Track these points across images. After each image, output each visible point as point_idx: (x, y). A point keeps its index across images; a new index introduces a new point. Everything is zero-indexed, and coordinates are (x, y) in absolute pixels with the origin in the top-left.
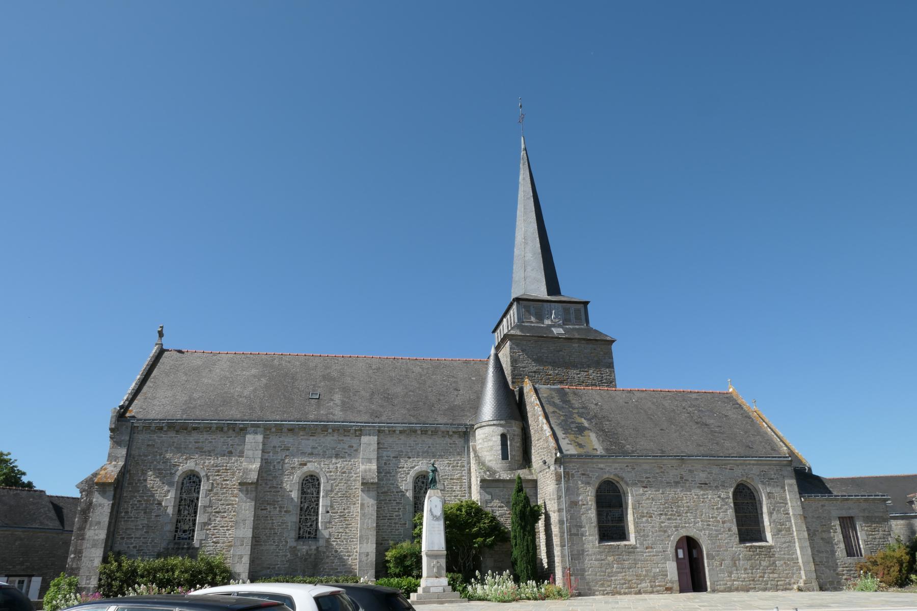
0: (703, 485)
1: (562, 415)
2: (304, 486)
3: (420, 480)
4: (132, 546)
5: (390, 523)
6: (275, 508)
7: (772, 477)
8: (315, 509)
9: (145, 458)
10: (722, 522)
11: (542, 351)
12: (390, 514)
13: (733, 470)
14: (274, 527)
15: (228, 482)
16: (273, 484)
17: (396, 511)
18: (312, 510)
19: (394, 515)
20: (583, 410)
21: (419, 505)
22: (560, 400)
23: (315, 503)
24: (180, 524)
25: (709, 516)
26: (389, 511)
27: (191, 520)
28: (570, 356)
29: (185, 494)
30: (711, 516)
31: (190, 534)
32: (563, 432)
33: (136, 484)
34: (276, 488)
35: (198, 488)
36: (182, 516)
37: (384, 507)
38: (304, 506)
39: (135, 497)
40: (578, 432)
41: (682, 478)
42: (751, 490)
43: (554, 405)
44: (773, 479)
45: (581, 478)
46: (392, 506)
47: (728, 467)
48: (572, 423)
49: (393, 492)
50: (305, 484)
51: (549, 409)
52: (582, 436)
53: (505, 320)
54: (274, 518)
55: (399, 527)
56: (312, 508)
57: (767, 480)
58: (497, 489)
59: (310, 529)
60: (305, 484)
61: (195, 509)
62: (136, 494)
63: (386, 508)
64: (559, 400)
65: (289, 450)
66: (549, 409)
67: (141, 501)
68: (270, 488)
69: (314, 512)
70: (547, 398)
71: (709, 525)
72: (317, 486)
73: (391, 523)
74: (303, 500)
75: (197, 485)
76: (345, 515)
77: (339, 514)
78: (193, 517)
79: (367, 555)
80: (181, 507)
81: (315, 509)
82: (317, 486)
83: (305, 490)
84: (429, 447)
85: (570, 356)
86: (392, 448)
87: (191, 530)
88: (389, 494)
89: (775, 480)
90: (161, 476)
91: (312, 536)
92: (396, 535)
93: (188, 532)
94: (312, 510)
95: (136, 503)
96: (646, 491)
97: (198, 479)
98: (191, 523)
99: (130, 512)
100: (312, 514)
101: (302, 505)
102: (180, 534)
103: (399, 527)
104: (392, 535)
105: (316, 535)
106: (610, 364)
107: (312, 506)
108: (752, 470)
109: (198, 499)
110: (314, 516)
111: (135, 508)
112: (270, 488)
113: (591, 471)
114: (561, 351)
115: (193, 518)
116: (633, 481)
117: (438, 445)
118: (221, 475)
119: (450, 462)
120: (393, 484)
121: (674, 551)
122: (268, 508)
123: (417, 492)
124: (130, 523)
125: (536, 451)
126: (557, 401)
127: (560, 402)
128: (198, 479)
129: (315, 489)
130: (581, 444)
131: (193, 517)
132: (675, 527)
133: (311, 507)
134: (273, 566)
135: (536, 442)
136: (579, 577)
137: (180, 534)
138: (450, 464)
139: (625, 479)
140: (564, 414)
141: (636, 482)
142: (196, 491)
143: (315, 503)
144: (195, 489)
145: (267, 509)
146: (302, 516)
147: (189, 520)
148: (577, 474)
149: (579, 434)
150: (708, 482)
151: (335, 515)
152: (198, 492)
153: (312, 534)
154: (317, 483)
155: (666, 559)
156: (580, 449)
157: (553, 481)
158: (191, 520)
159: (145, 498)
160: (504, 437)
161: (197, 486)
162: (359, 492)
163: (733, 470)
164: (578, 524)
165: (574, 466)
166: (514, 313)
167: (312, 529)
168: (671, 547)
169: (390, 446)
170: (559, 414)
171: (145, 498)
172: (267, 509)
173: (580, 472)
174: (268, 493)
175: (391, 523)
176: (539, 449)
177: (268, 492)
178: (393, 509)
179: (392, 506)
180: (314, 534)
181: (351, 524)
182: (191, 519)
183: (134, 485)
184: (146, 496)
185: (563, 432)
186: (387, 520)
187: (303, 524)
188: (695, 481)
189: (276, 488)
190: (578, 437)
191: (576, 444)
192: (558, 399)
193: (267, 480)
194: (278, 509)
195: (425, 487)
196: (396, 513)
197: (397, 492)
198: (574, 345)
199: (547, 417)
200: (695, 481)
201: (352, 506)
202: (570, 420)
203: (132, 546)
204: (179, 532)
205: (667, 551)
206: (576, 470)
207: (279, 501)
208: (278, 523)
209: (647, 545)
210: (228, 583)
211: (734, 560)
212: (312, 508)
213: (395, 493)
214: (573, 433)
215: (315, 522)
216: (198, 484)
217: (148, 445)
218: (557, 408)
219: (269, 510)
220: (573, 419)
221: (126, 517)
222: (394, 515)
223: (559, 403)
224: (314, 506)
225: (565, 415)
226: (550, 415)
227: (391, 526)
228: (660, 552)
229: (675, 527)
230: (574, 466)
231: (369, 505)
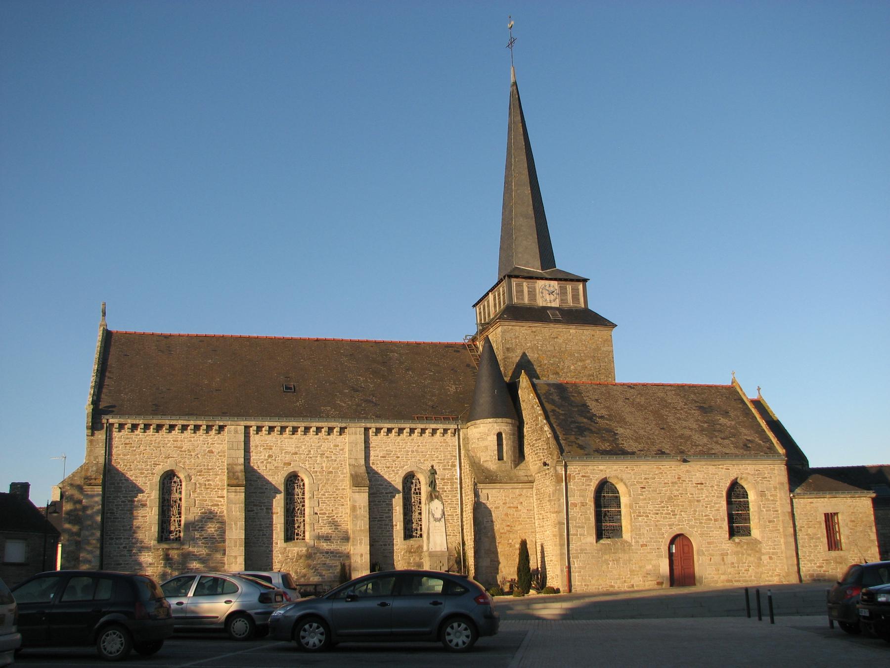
0: (699, 485)
1: (562, 414)
2: (288, 487)
3: (409, 480)
4: (122, 546)
5: (380, 525)
6: (262, 509)
7: (766, 476)
8: (301, 510)
9: (124, 457)
10: (714, 519)
11: (537, 338)
12: (379, 515)
13: (729, 469)
14: (262, 528)
15: (211, 482)
16: (258, 485)
17: (387, 513)
18: (299, 511)
19: (384, 517)
20: (582, 408)
21: (409, 506)
22: (559, 397)
23: (301, 504)
24: (165, 525)
25: (702, 514)
26: (378, 513)
27: (176, 521)
28: (566, 344)
29: (167, 494)
30: (704, 514)
31: (176, 534)
32: (564, 433)
33: (118, 483)
34: (261, 488)
35: (179, 489)
36: (167, 516)
37: (374, 509)
38: (290, 507)
39: (118, 497)
40: (578, 433)
41: (679, 478)
42: (744, 489)
43: (553, 402)
44: (766, 478)
45: (582, 480)
46: (381, 507)
47: (625, 466)
48: (572, 422)
49: (382, 493)
50: (290, 485)
51: (548, 407)
52: (582, 437)
53: (491, 296)
54: (261, 520)
55: (389, 528)
56: (298, 509)
57: (760, 479)
58: (494, 491)
59: (298, 531)
60: (290, 485)
61: (179, 510)
62: (119, 494)
63: (376, 510)
64: (557, 398)
65: (272, 449)
66: (548, 407)
67: (125, 502)
68: (255, 488)
69: (301, 513)
70: (545, 394)
71: (701, 523)
72: (302, 487)
73: (382, 525)
74: (288, 501)
75: (178, 485)
76: (334, 516)
77: (327, 515)
78: (177, 517)
79: (362, 555)
80: (165, 508)
81: (301, 510)
82: (302, 487)
83: (290, 491)
84: (419, 446)
85: (566, 344)
86: (380, 447)
87: (177, 531)
88: (378, 495)
89: (768, 479)
90: (143, 476)
91: (301, 537)
92: (387, 536)
93: (175, 533)
94: (299, 511)
95: (120, 503)
96: (644, 492)
97: (179, 479)
98: (177, 524)
99: (116, 513)
100: (299, 515)
101: (288, 507)
102: (166, 535)
103: (389, 528)
104: (383, 536)
105: (304, 536)
106: (609, 352)
107: (298, 507)
108: (747, 469)
109: (180, 499)
110: (301, 517)
111: (120, 509)
112: (255, 488)
113: (592, 473)
114: (557, 338)
115: (178, 519)
116: (631, 482)
117: (427, 444)
118: (204, 475)
119: (439, 461)
120: (382, 485)
121: (667, 548)
122: (255, 509)
123: (406, 493)
124: (117, 524)
125: (534, 451)
126: (556, 398)
127: (559, 399)
128: (179, 479)
129: (300, 490)
130: (582, 445)
131: (177, 517)
132: (669, 525)
133: (297, 509)
134: (265, 567)
135: (534, 442)
136: (577, 574)
137: (166, 535)
138: (441, 463)
139: (624, 480)
140: (563, 412)
141: (635, 483)
142: (178, 491)
143: (301, 504)
144: (176, 489)
145: (254, 511)
146: (288, 517)
147: (174, 521)
148: (578, 476)
149: (579, 435)
150: (703, 482)
151: (324, 516)
152: (181, 493)
153: (300, 535)
154: (302, 484)
155: (661, 556)
156: (581, 451)
157: (554, 483)
158: (176, 521)
159: (129, 498)
160: (499, 435)
161: (179, 486)
162: (348, 491)
163: (729, 469)
164: (577, 525)
165: (575, 469)
166: (503, 291)
167: (300, 530)
168: (665, 545)
169: (377, 445)
170: (558, 412)
171: (129, 498)
172: (254, 511)
173: (581, 474)
174: (254, 494)
175: (382, 525)
176: (537, 450)
177: (253, 493)
178: (382, 510)
179: (381, 507)
180: (302, 536)
181: (341, 526)
182: (176, 519)
183: (116, 485)
184: (129, 497)
185: (564, 433)
186: (376, 522)
187: (291, 526)
188: (692, 481)
189: (261, 488)
190: (579, 438)
191: (577, 445)
192: (557, 396)
193: (251, 480)
194: (265, 510)
195: (414, 487)
196: (387, 515)
197: (386, 493)
198: (571, 331)
199: (547, 418)
200: (692, 481)
201: (340, 507)
202: (570, 420)
203: (122, 546)
204: (165, 533)
205: (661, 549)
206: (577, 472)
207: (265, 503)
208: (266, 524)
209: (642, 543)
210: (764, 429)
211: (723, 555)
212: (298, 509)
213: (384, 494)
214: (573, 433)
215: (302, 524)
216: (180, 484)
217: (126, 444)
218: (556, 406)
219: (256, 511)
220: (573, 418)
221: (113, 517)
222: (384, 517)
223: (557, 400)
224: (301, 507)
225: (565, 414)
226: (550, 414)
227: (382, 528)
228: (654, 549)
229: (669, 525)
230: (575, 469)
231: (360, 507)
